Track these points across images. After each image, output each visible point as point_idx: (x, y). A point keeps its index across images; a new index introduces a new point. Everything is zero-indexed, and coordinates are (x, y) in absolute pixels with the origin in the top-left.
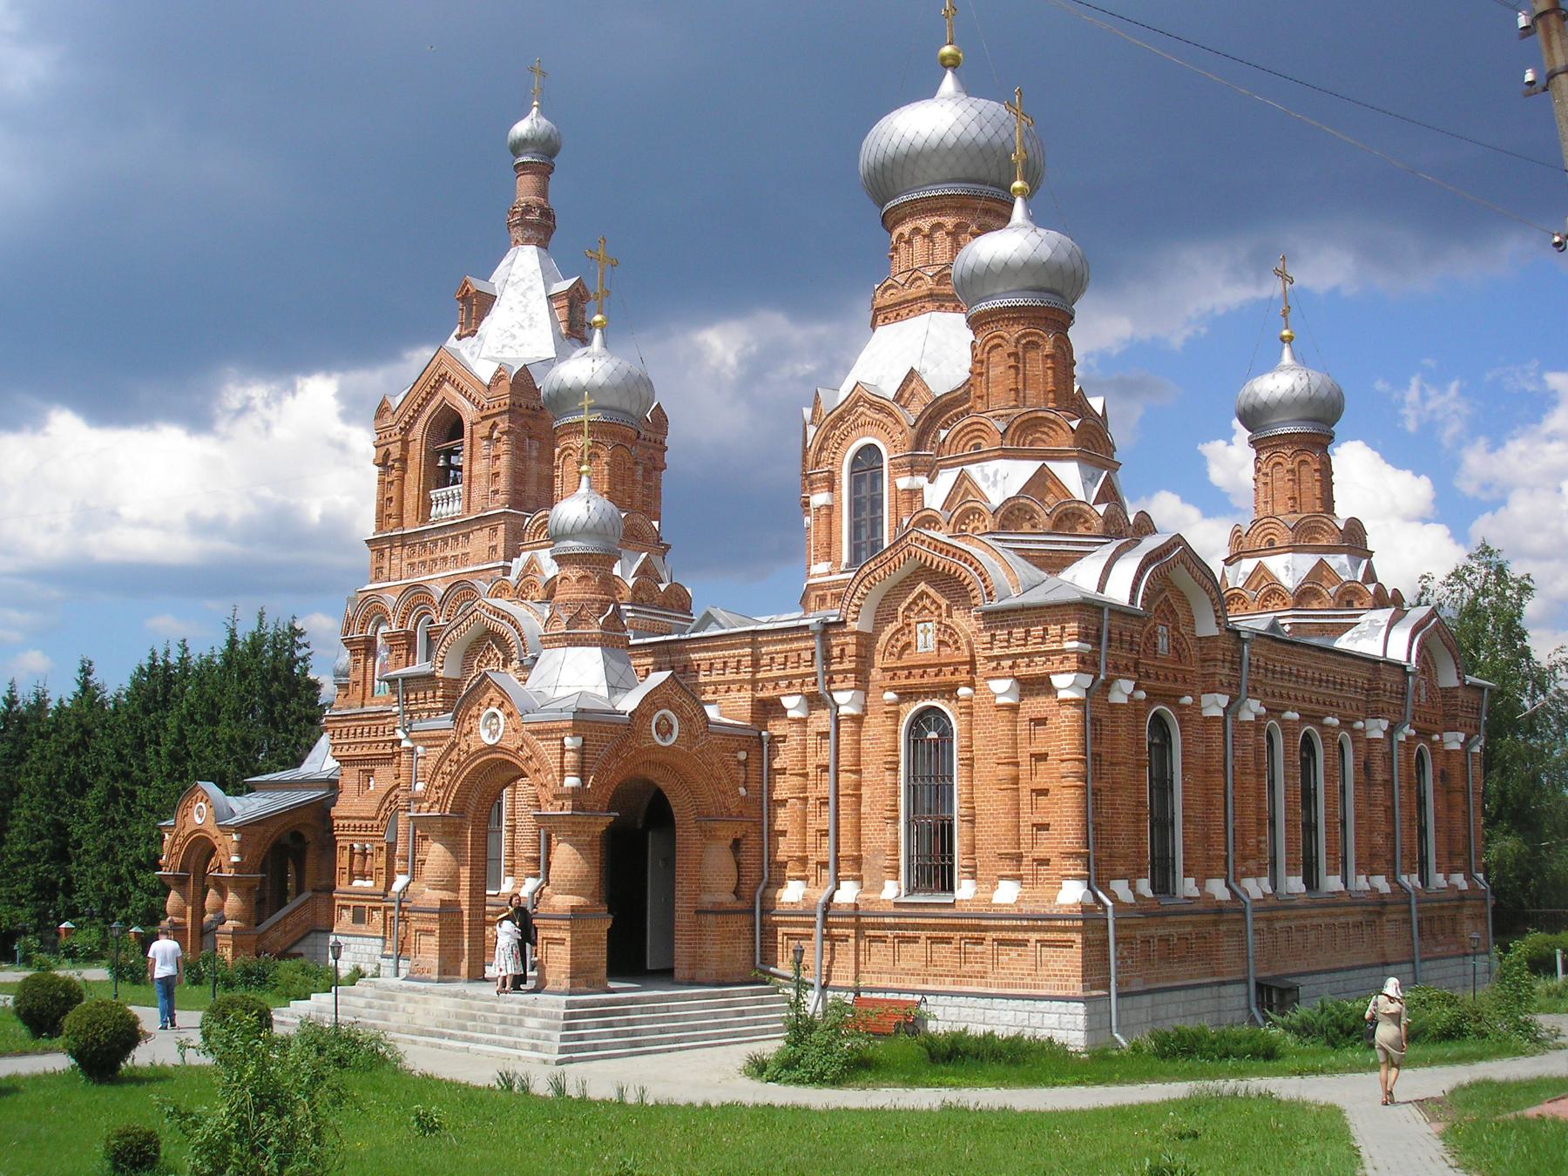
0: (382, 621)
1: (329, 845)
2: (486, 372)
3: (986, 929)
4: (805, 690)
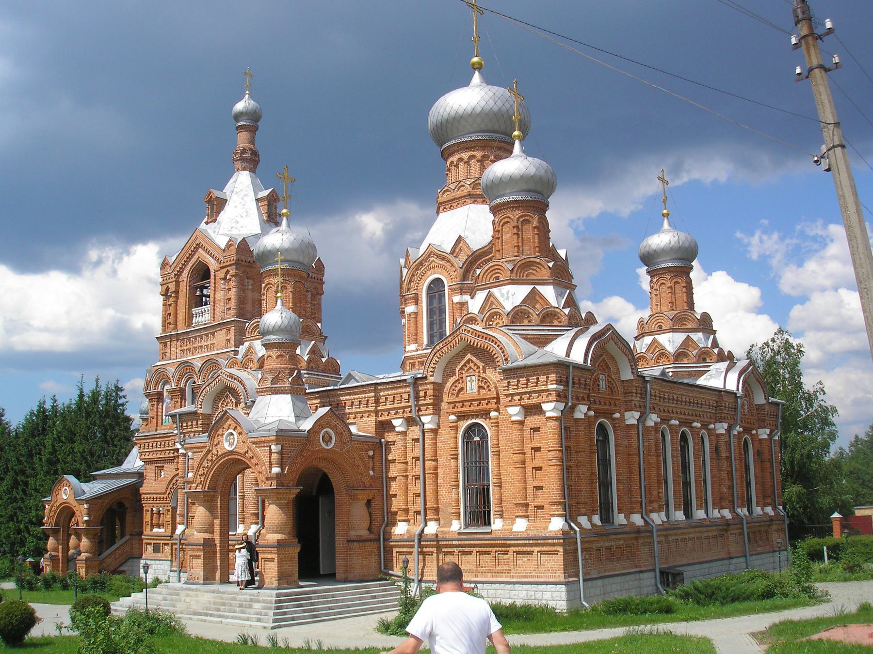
0: (167, 382)
2: (222, 242)
3: (509, 546)
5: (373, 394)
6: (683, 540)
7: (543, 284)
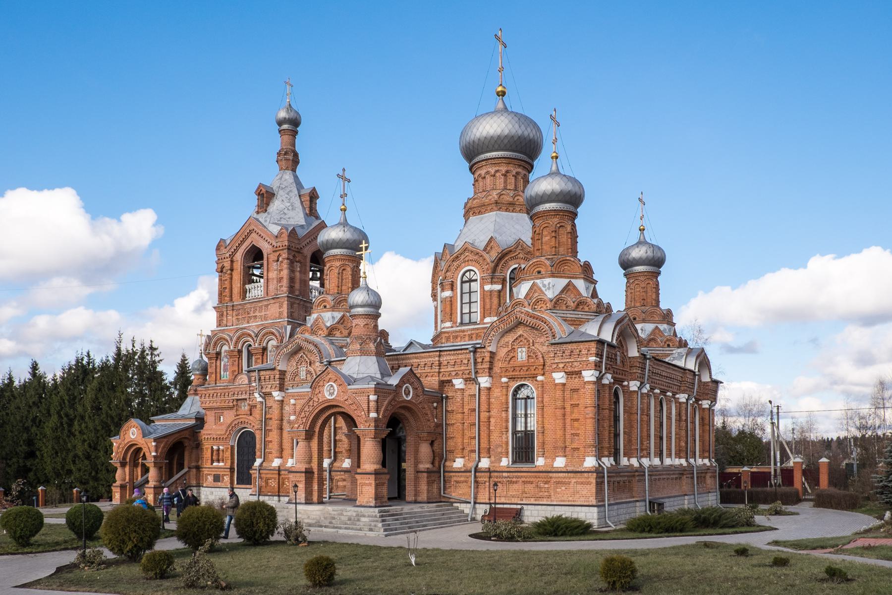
1: (198, 446)
2: (275, 229)
6: (659, 479)
7: (576, 278)
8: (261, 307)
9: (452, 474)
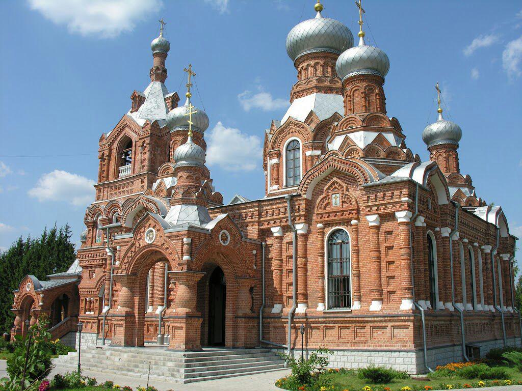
0: (100, 215)
1: (77, 298)
2: (141, 122)
3: (367, 322)
4: (282, 224)
5: (257, 209)
8: (128, 183)
9: (270, 320)
